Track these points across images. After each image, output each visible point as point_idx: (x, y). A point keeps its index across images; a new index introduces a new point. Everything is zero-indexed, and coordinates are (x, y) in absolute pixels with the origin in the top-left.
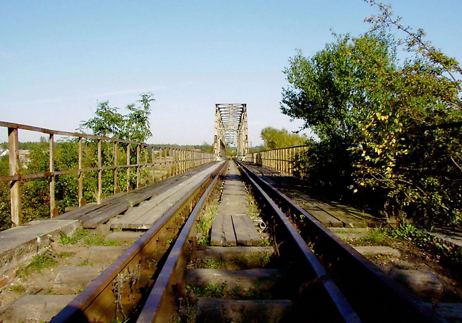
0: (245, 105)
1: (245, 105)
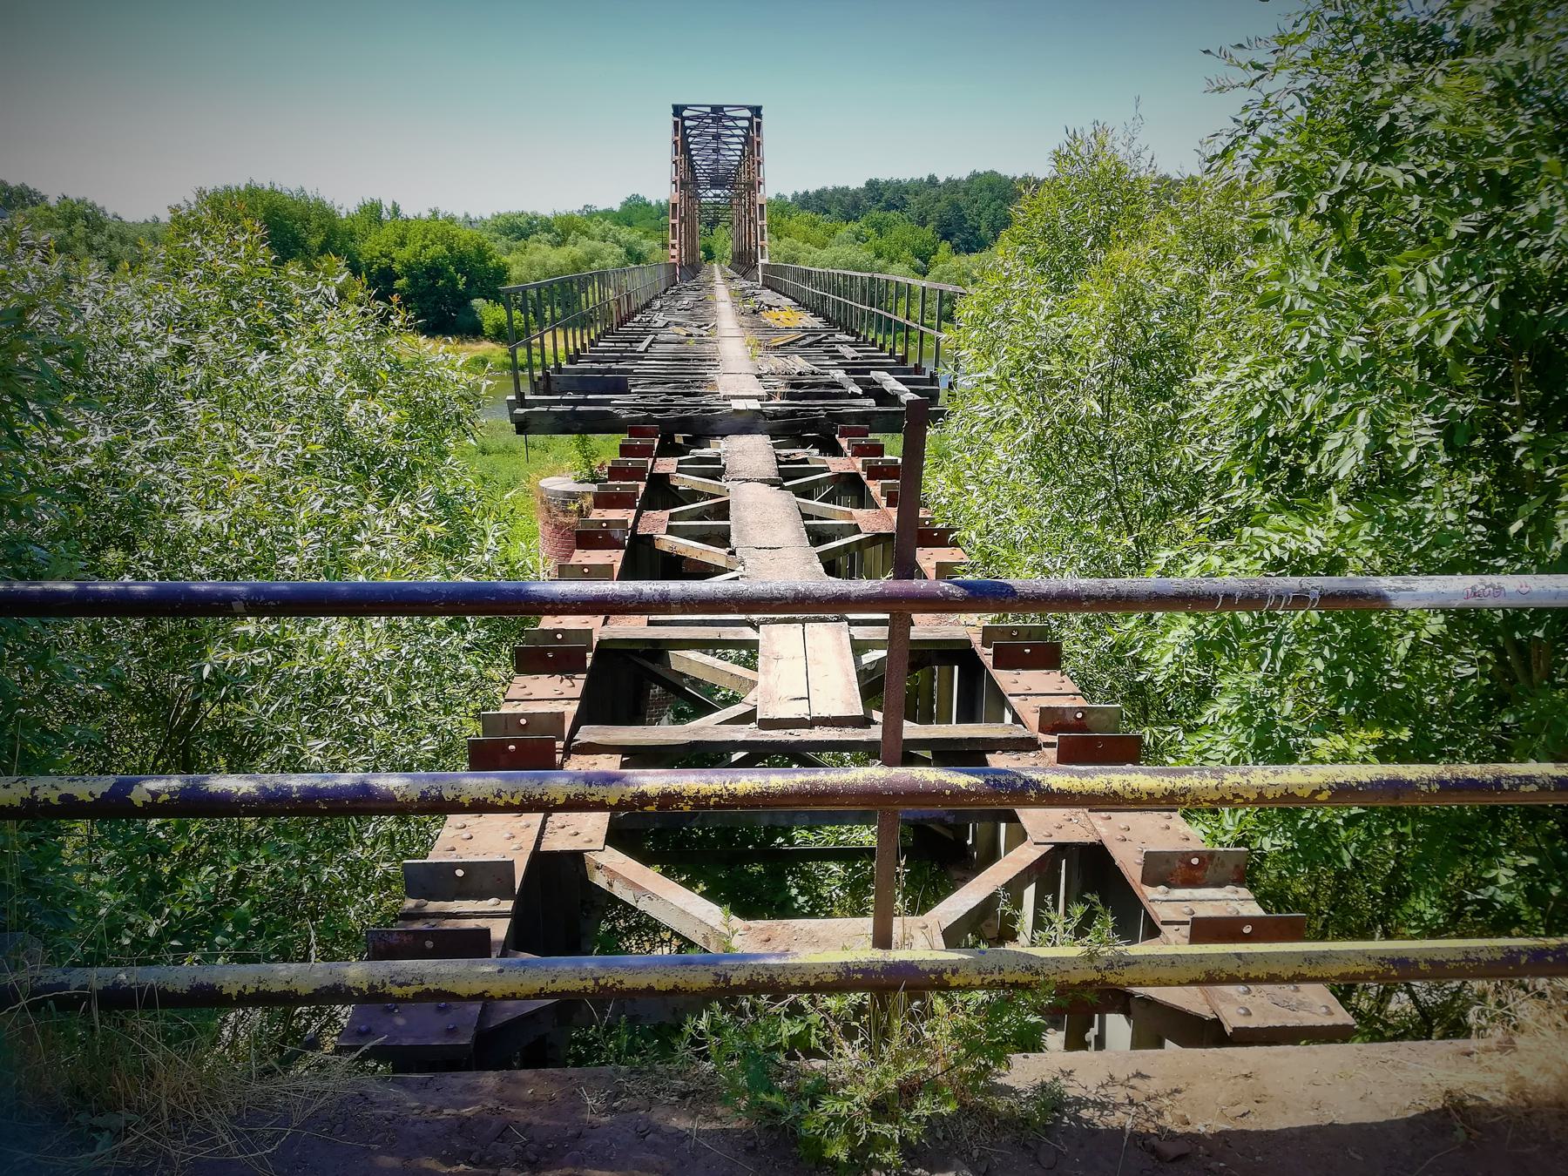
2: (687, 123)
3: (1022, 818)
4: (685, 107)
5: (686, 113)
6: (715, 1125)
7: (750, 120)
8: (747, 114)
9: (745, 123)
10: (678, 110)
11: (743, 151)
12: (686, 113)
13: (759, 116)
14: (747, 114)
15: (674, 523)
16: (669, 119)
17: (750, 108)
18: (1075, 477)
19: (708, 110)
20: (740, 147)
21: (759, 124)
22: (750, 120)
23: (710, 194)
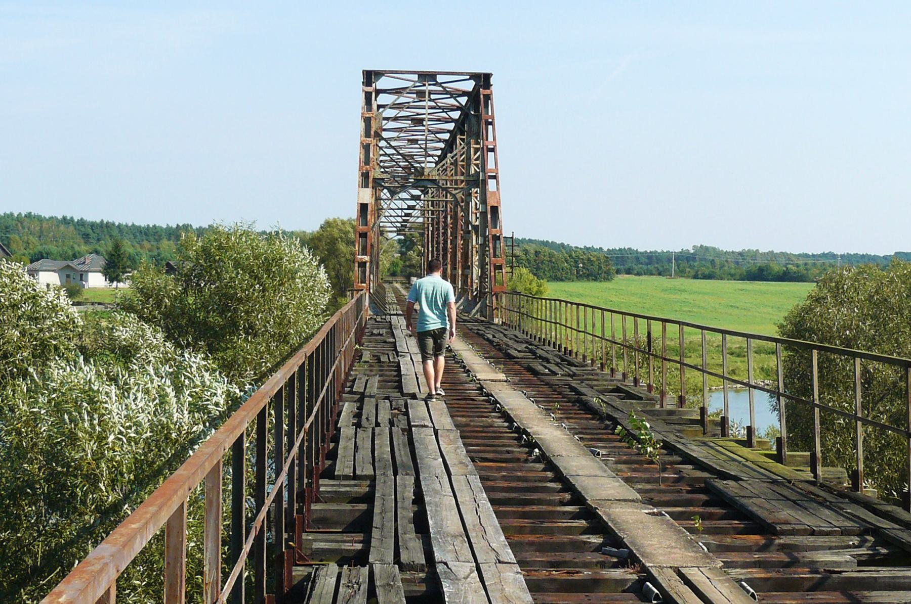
0: (487, 77)
1: (487, 77)
4: (379, 74)
5: (382, 84)
8: (469, 86)
10: (370, 77)
12: (382, 84)
17: (474, 76)
21: (488, 97)
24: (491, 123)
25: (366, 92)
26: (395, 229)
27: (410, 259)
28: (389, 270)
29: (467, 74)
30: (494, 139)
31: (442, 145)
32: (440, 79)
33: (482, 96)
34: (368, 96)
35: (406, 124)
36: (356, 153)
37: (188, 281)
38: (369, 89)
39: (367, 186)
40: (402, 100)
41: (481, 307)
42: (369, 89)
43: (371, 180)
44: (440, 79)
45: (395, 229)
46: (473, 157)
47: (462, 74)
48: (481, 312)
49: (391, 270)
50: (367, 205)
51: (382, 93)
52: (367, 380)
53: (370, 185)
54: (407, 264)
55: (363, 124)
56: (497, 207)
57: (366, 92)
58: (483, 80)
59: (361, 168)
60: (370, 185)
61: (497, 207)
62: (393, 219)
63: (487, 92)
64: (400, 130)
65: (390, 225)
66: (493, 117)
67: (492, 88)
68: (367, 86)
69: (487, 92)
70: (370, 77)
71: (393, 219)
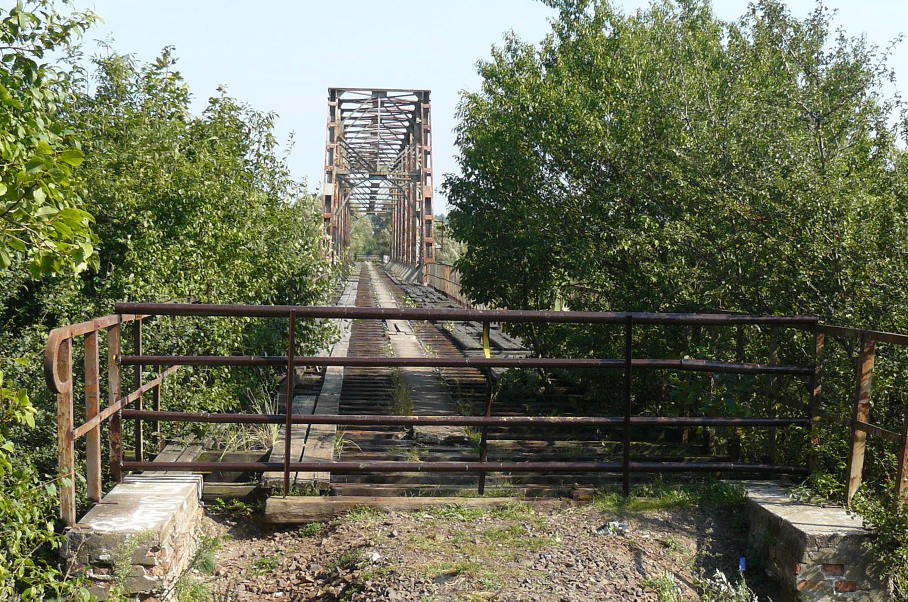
0: (427, 93)
1: (427, 93)
2: (344, 106)
3: (39, 190)
4: (341, 91)
5: (344, 96)
6: (819, 584)
7: (417, 104)
8: (415, 99)
9: (412, 108)
10: (334, 93)
11: (407, 135)
12: (344, 96)
13: (427, 101)
14: (415, 99)
15: (70, 345)
16: (324, 103)
17: (417, 93)
18: (859, 322)
19: (370, 93)
20: (405, 131)
21: (427, 111)
22: (417, 104)
23: (368, 183)
24: (429, 131)
25: (331, 106)
26: (365, 209)
27: (384, 237)
28: (364, 248)
29: (412, 91)
30: (431, 144)
31: (400, 142)
32: (389, 94)
33: (422, 110)
34: (332, 109)
35: (369, 122)
36: (324, 156)
37: (313, 230)
38: (333, 104)
39: (330, 182)
40: (364, 106)
41: (418, 275)
42: (333, 104)
43: (334, 177)
44: (389, 94)
45: (365, 209)
46: (418, 155)
47: (407, 91)
48: (418, 279)
49: (368, 248)
50: (330, 196)
51: (331, 133)
52: (437, 579)
53: (333, 181)
54: (381, 241)
55: (329, 132)
56: (430, 198)
57: (331, 106)
58: (424, 96)
59: (326, 167)
60: (333, 181)
61: (430, 198)
62: (363, 201)
63: (426, 106)
64: (365, 126)
65: (362, 206)
66: (430, 127)
67: (431, 103)
68: (331, 101)
69: (426, 106)
70: (334, 93)
71: (363, 201)
